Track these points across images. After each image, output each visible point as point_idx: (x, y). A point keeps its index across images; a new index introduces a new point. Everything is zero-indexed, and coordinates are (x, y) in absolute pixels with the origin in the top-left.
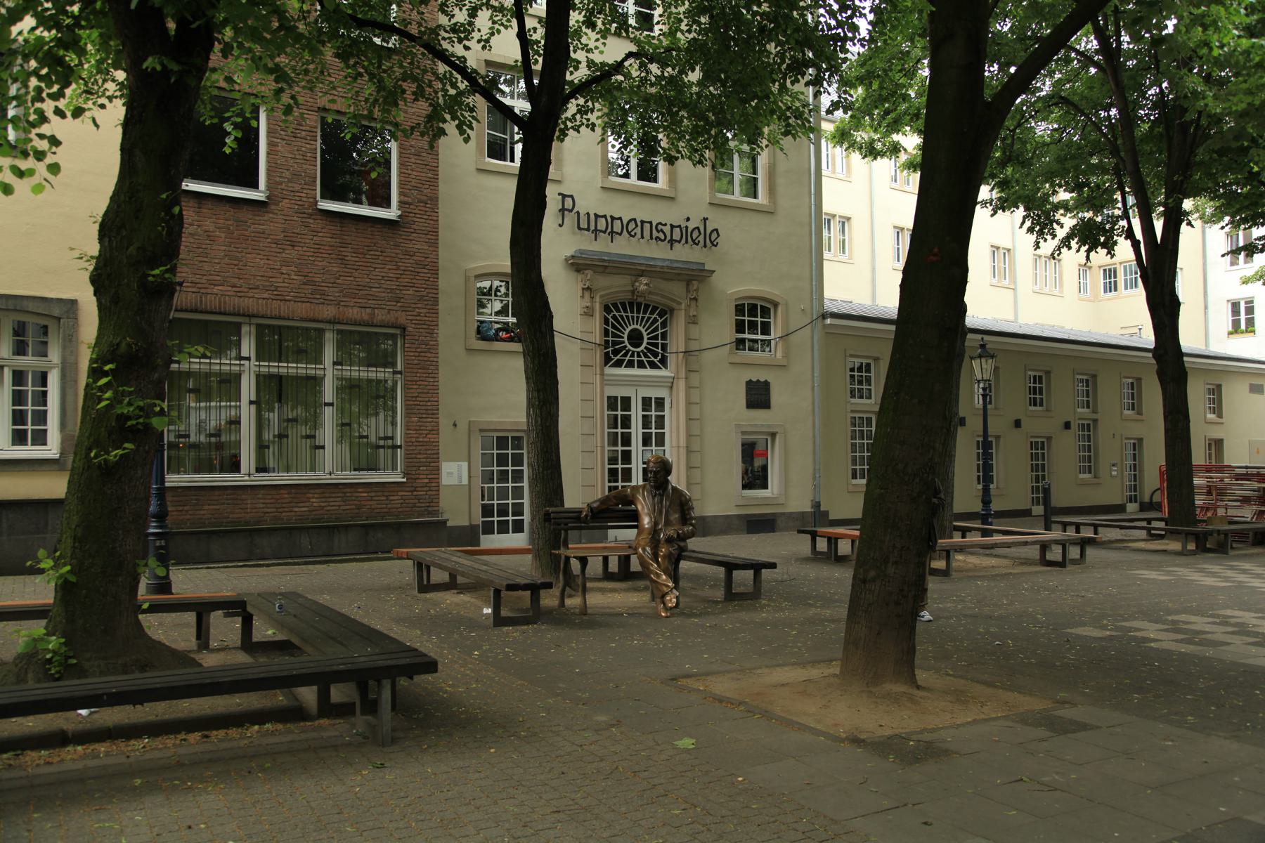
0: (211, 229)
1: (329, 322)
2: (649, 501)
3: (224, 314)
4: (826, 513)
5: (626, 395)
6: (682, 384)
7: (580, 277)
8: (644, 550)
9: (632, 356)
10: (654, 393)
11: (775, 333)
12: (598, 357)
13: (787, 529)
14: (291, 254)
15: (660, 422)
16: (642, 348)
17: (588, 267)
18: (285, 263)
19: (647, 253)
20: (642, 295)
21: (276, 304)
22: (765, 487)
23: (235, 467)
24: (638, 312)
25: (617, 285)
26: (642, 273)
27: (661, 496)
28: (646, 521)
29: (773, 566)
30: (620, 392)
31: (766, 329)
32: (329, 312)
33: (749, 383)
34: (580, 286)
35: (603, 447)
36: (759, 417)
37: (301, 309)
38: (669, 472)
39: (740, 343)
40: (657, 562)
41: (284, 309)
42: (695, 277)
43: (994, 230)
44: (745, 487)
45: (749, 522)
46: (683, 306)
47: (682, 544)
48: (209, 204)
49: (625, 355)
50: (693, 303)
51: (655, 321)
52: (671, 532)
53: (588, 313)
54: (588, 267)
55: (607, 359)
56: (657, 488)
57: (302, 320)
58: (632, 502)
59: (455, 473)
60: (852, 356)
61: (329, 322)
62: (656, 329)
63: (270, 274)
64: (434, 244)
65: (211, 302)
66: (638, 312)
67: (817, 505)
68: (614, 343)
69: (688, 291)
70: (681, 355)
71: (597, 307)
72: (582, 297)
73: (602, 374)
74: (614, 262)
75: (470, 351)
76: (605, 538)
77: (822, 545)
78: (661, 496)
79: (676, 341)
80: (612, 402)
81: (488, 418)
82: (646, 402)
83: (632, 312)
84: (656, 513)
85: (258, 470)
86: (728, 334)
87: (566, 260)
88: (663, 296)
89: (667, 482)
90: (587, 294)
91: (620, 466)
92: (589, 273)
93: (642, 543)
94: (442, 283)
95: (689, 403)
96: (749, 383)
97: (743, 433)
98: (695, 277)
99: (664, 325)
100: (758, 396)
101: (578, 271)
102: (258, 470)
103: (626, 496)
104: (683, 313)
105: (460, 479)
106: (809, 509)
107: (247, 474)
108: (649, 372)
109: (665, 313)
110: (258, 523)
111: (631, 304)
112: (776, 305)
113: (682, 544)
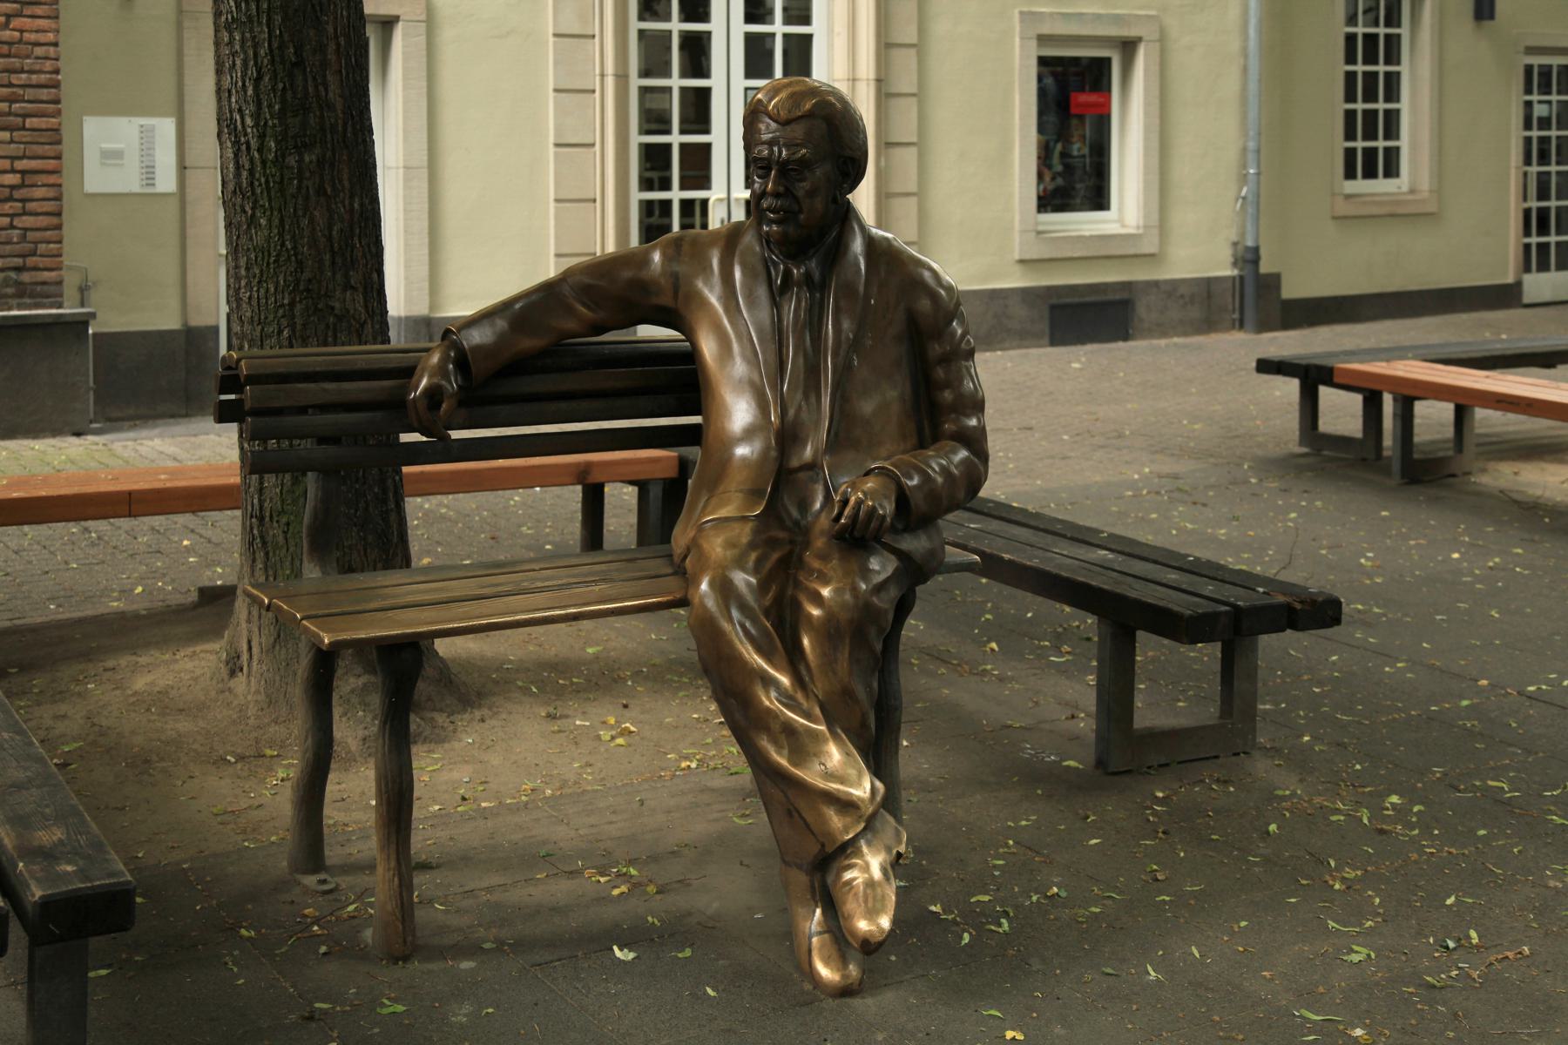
2: (756, 317)
4: (1271, 284)
8: (724, 589)
13: (1162, 330)
27: (816, 287)
29: (1321, 613)
35: (622, 78)
38: (853, 172)
40: (793, 658)
43: (908, 41)
45: (1053, 308)
47: (916, 544)
52: (865, 492)
67: (1249, 258)
77: (1341, 412)
78: (816, 287)
84: (789, 369)
89: (847, 214)
91: (675, 139)
93: (716, 547)
97: (1043, 39)
105: (149, 174)
106: (1224, 269)
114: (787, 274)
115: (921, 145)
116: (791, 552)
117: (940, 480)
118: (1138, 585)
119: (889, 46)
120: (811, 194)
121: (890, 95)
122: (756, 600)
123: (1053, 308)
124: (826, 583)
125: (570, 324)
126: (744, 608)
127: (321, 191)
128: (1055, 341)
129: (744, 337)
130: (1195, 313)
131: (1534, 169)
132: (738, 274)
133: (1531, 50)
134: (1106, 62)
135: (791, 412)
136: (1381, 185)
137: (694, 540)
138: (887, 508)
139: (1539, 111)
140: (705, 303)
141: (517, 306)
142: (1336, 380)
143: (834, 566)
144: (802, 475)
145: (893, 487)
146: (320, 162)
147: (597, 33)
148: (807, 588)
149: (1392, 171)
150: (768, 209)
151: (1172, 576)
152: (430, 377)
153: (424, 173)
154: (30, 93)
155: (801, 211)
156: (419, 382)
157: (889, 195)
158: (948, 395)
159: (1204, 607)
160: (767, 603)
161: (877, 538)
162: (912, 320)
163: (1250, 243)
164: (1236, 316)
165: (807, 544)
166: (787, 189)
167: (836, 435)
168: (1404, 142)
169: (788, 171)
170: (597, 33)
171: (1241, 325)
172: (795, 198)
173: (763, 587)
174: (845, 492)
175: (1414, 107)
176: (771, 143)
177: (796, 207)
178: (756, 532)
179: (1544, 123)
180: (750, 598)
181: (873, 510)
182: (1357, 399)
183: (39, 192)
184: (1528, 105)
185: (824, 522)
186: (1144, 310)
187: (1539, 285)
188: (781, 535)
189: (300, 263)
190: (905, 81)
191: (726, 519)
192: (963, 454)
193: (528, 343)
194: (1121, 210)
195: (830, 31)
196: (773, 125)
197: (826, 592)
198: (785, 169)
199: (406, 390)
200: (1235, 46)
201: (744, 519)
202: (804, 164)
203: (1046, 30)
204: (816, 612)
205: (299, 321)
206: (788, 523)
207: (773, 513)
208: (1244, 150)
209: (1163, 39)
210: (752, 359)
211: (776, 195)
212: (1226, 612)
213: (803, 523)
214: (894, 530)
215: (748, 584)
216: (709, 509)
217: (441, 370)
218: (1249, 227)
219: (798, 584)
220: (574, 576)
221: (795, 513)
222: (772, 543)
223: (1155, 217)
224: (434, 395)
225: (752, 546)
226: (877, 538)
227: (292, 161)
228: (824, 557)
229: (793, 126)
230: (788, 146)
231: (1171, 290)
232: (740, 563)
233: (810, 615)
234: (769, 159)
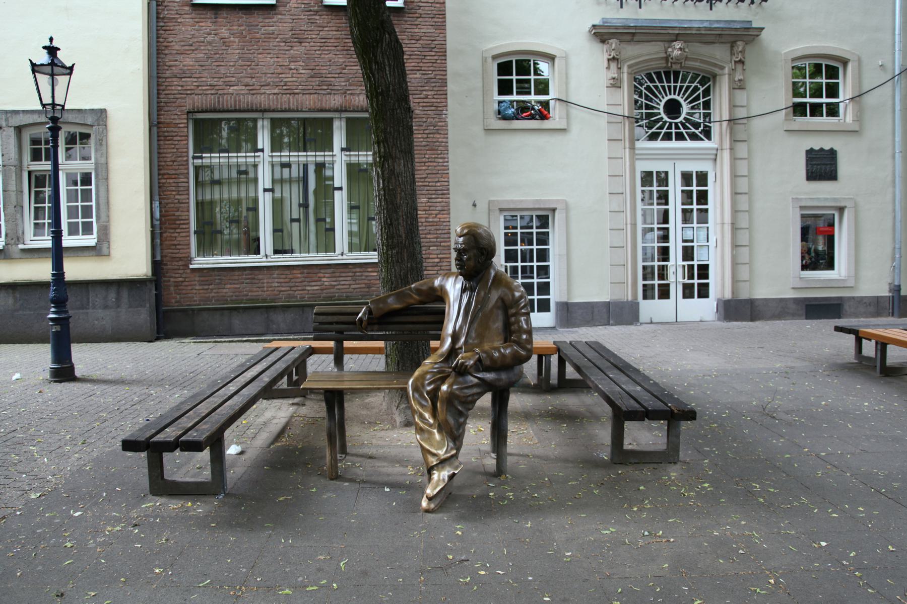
0: (226, 35)
1: (336, 110)
3: (240, 111)
6: (726, 155)
7: (605, 47)
9: (670, 127)
10: (694, 167)
11: (845, 92)
14: (298, 50)
15: (703, 197)
16: (681, 119)
17: (613, 35)
18: (294, 59)
19: (683, 16)
20: (677, 61)
21: (285, 98)
22: (830, 266)
23: (254, 247)
24: (676, 81)
25: (648, 53)
26: (677, 37)
30: (655, 167)
31: (833, 91)
32: (336, 101)
33: (810, 153)
34: (606, 56)
36: (823, 191)
37: (309, 101)
39: (799, 110)
41: (293, 102)
42: (740, 38)
44: (804, 267)
45: (807, 306)
46: (726, 71)
48: (224, 14)
49: (661, 128)
50: (739, 66)
51: (696, 89)
53: (615, 84)
54: (613, 35)
57: (310, 111)
61: (336, 110)
62: (697, 98)
63: (280, 71)
64: (441, 27)
65: (228, 101)
66: (676, 81)
67: (897, 289)
69: (732, 54)
70: (725, 124)
71: (625, 77)
72: (608, 68)
73: (632, 148)
74: (641, 27)
75: (488, 130)
77: (869, 349)
79: (721, 108)
80: (647, 178)
81: (509, 197)
82: (687, 178)
83: (669, 81)
85: (276, 252)
86: (784, 98)
87: (590, 32)
88: (702, 61)
90: (613, 65)
92: (614, 42)
94: (452, 65)
95: (734, 176)
96: (810, 153)
97: (802, 208)
98: (740, 38)
99: (707, 92)
100: (822, 166)
101: (603, 41)
102: (276, 252)
104: (725, 80)
107: (266, 257)
108: (689, 144)
109: (707, 80)
110: (273, 301)
111: (667, 74)
112: (845, 62)
115: (750, 246)
119: (736, 211)
121: (737, 229)
123: (807, 306)
125: (412, 301)
127: (397, 261)
128: (808, 317)
130: (872, 309)
134: (547, 216)
146: (397, 253)
153: (565, 257)
154: (442, 236)
157: (737, 264)
171: (893, 315)
183: (445, 264)
186: (846, 307)
189: (392, 283)
190: (743, 222)
194: (839, 270)
195: (715, 207)
200: (890, 208)
203: (803, 204)
208: (894, 248)
209: (856, 207)
218: (896, 277)
223: (853, 273)
224: (361, 319)
227: (390, 252)
231: (861, 300)
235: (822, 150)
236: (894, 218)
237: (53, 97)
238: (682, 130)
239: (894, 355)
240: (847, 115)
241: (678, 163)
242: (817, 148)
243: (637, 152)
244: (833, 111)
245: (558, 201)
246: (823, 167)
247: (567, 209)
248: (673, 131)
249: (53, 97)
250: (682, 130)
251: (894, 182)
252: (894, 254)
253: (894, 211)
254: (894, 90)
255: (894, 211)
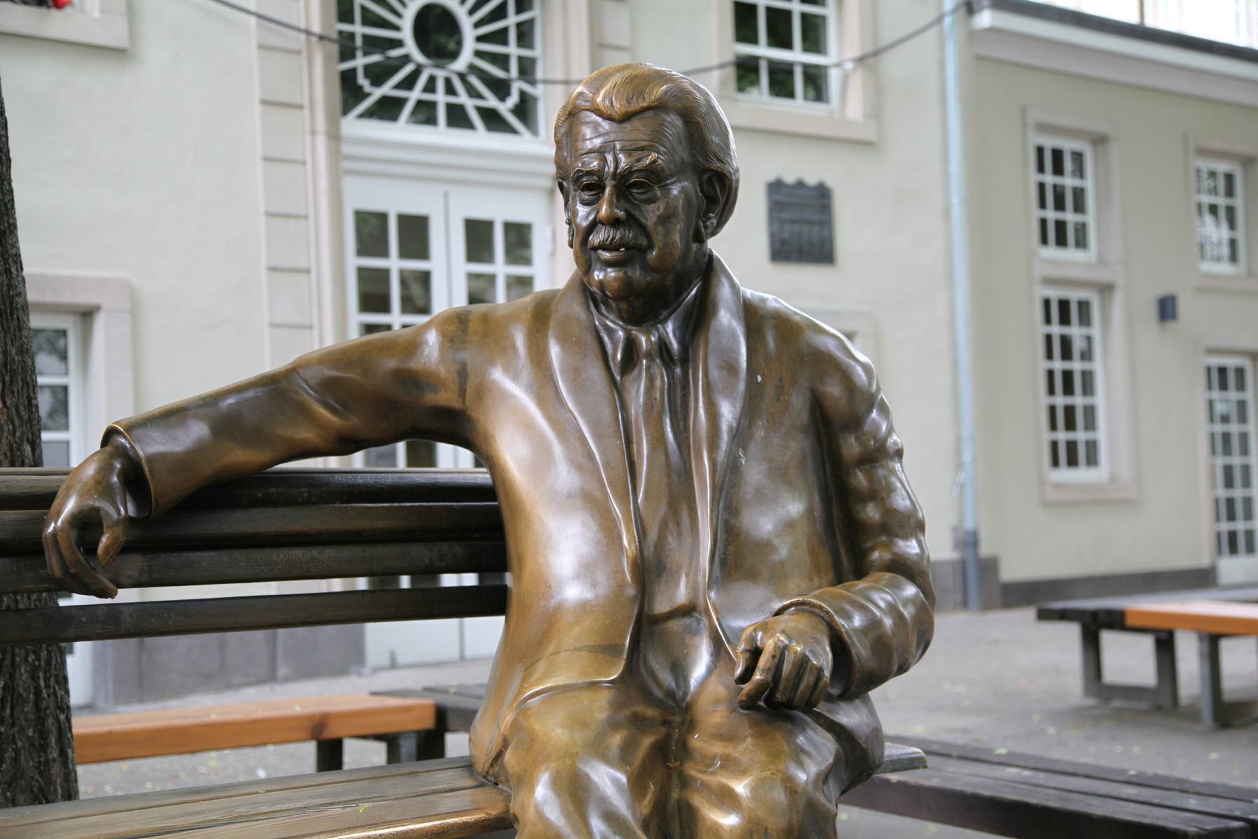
4: (989, 567)
5: (414, 208)
8: (576, 791)
9: (430, 87)
12: (316, 78)
16: (461, 64)
28: (565, 555)
30: (396, 201)
47: (849, 716)
49: (408, 83)
55: (350, 91)
56: (640, 305)
58: (458, 426)
59: (786, 748)
60: (1042, 128)
68: (373, 44)
73: (334, 136)
75: (1024, 110)
76: (353, 660)
77: (1128, 659)
78: (679, 362)
80: (371, 232)
84: (652, 494)
89: (708, 269)
93: (554, 729)
103: (412, 380)
108: (480, 138)
113: (849, 716)
114: (631, 347)
116: (668, 737)
117: (888, 622)
118: (1095, 801)
120: (665, 220)
122: (632, 807)
124: (741, 772)
126: (611, 817)
129: (565, 429)
131: (1220, 461)
132: (555, 351)
133: (1212, 351)
135: (653, 535)
136: (1082, 474)
137: (515, 723)
138: (824, 659)
139: (1220, 408)
140: (504, 395)
141: (231, 401)
142: (1130, 621)
143: (746, 748)
144: (675, 625)
145: (824, 629)
147: (316, 322)
148: (705, 785)
149: (1092, 460)
150: (603, 246)
151: (1130, 791)
152: (81, 496)
155: (651, 246)
156: (63, 505)
158: (872, 513)
159: (1212, 824)
160: (646, 811)
161: (808, 706)
162: (818, 406)
163: (969, 525)
164: (959, 597)
165: (690, 725)
166: (629, 214)
167: (723, 563)
168: (1101, 435)
169: (633, 187)
170: (316, 322)
171: (965, 605)
172: (643, 228)
173: (637, 786)
174: (752, 639)
175: (1109, 399)
176: (601, 152)
177: (643, 241)
178: (616, 706)
179: (1225, 419)
180: (620, 804)
181: (803, 663)
182: (1146, 644)
184: (1211, 403)
185: (719, 688)
187: (1232, 568)
188: (650, 712)
191: (566, 688)
192: (910, 590)
193: (241, 456)
196: (606, 125)
197: (741, 787)
198: (626, 185)
199: (43, 523)
201: (593, 685)
202: (654, 178)
204: (729, 820)
205: (8, 657)
206: (658, 693)
207: (634, 680)
208: (958, 440)
210: (583, 461)
211: (614, 223)
212: (1241, 829)
213: (679, 694)
214: (830, 699)
215: (615, 782)
216: (537, 675)
217: (101, 486)
219: (685, 782)
220: (321, 796)
221: (667, 679)
222: (639, 723)
224: (87, 524)
225: (613, 725)
226: (808, 706)
228: (728, 737)
229: (636, 122)
230: (628, 151)
232: (598, 751)
233: (716, 830)
234: (599, 173)
235: (800, 184)
236: (955, 364)
237: (1142, 16)
238: (463, 99)
239: (1242, 665)
240: (848, 101)
241: (456, 194)
242: (790, 179)
243: (347, 149)
244: (816, 81)
245: (104, 283)
246: (805, 228)
247: (135, 309)
248: (441, 98)
249: (1142, 16)
250: (463, 99)
251: (950, 275)
252: (958, 452)
253: (954, 347)
254: (942, 49)
255: (954, 347)
